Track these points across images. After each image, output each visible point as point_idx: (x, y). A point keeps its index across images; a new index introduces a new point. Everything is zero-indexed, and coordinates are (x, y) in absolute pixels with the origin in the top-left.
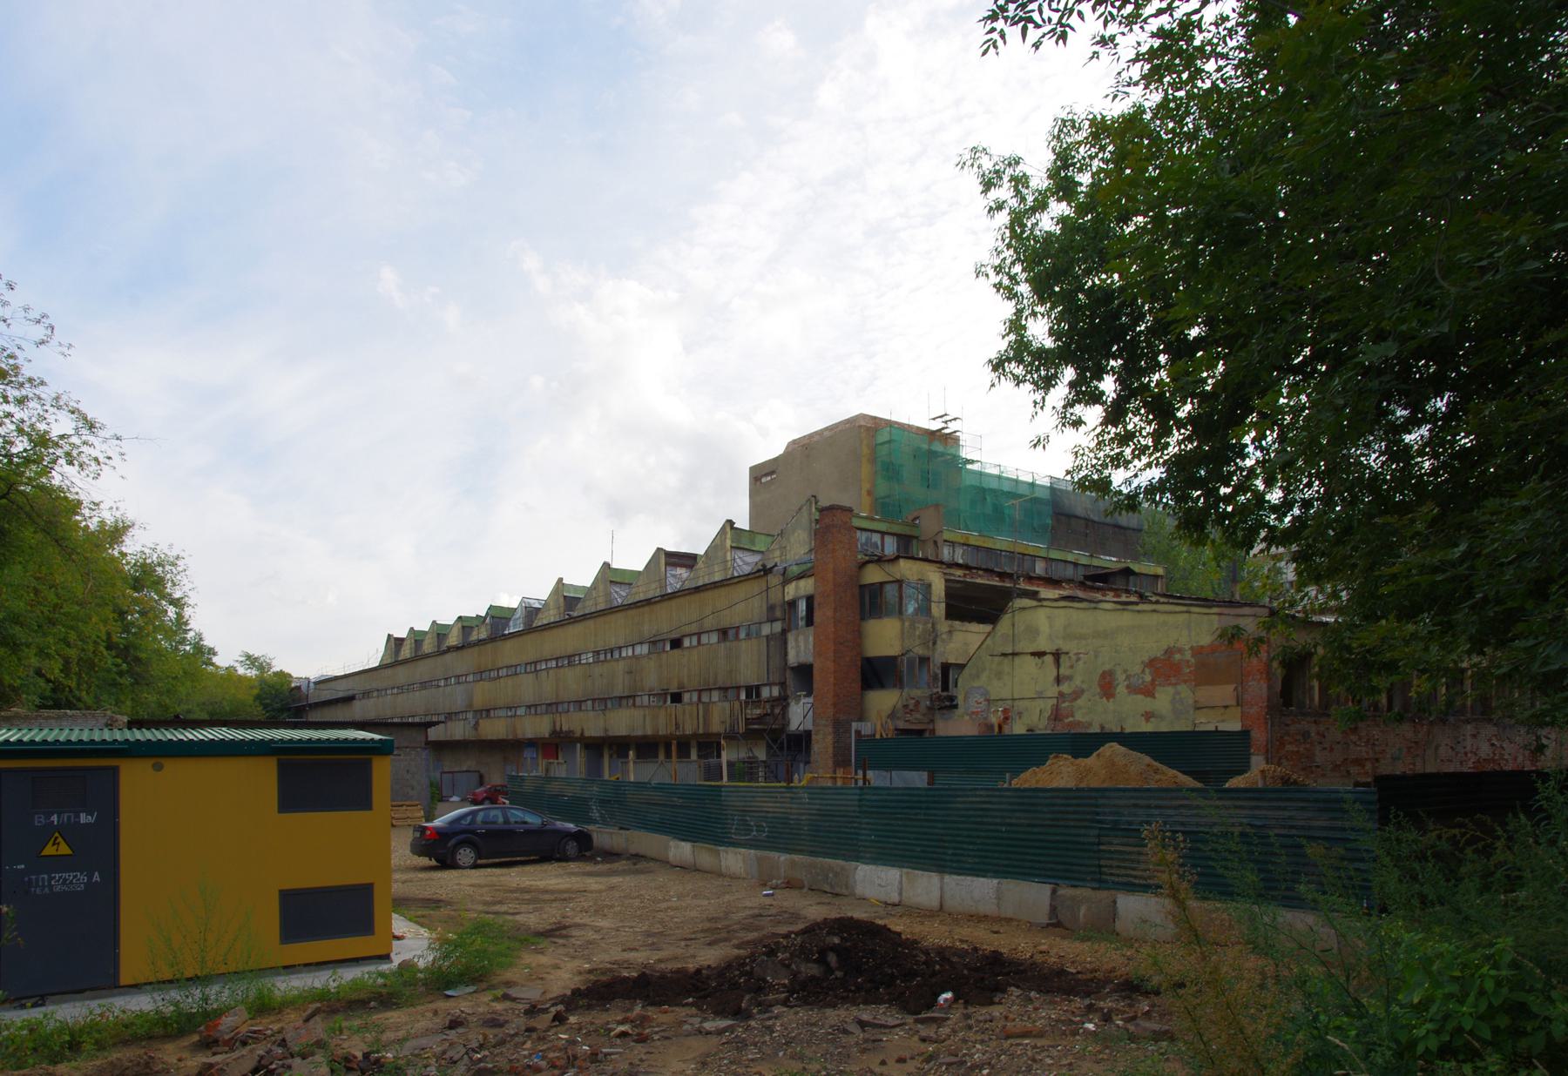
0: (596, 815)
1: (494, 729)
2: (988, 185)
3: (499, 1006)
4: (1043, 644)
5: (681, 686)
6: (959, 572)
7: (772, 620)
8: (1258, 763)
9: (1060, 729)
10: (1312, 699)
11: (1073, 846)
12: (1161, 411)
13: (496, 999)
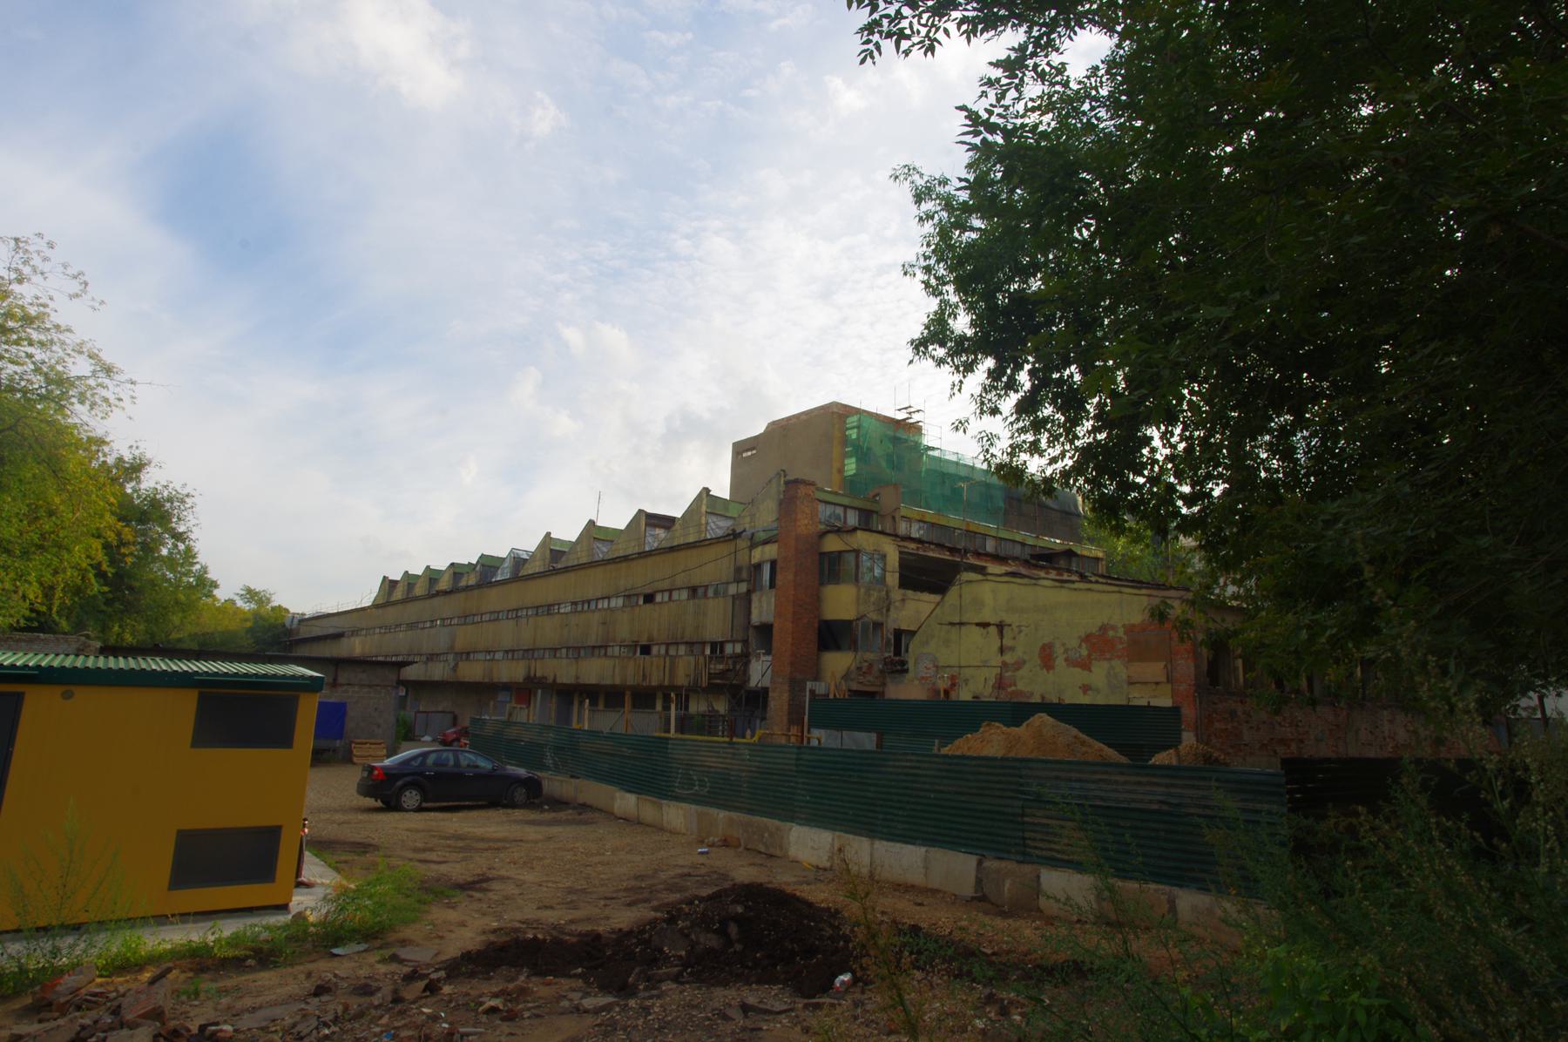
0: (549, 762)
1: (472, 672)
2: (919, 198)
3: (382, 969)
4: (987, 615)
5: (650, 639)
6: (913, 545)
7: (738, 581)
8: (1188, 738)
9: (1003, 697)
10: (1237, 680)
11: (988, 815)
12: (1072, 404)
13: (383, 961)
